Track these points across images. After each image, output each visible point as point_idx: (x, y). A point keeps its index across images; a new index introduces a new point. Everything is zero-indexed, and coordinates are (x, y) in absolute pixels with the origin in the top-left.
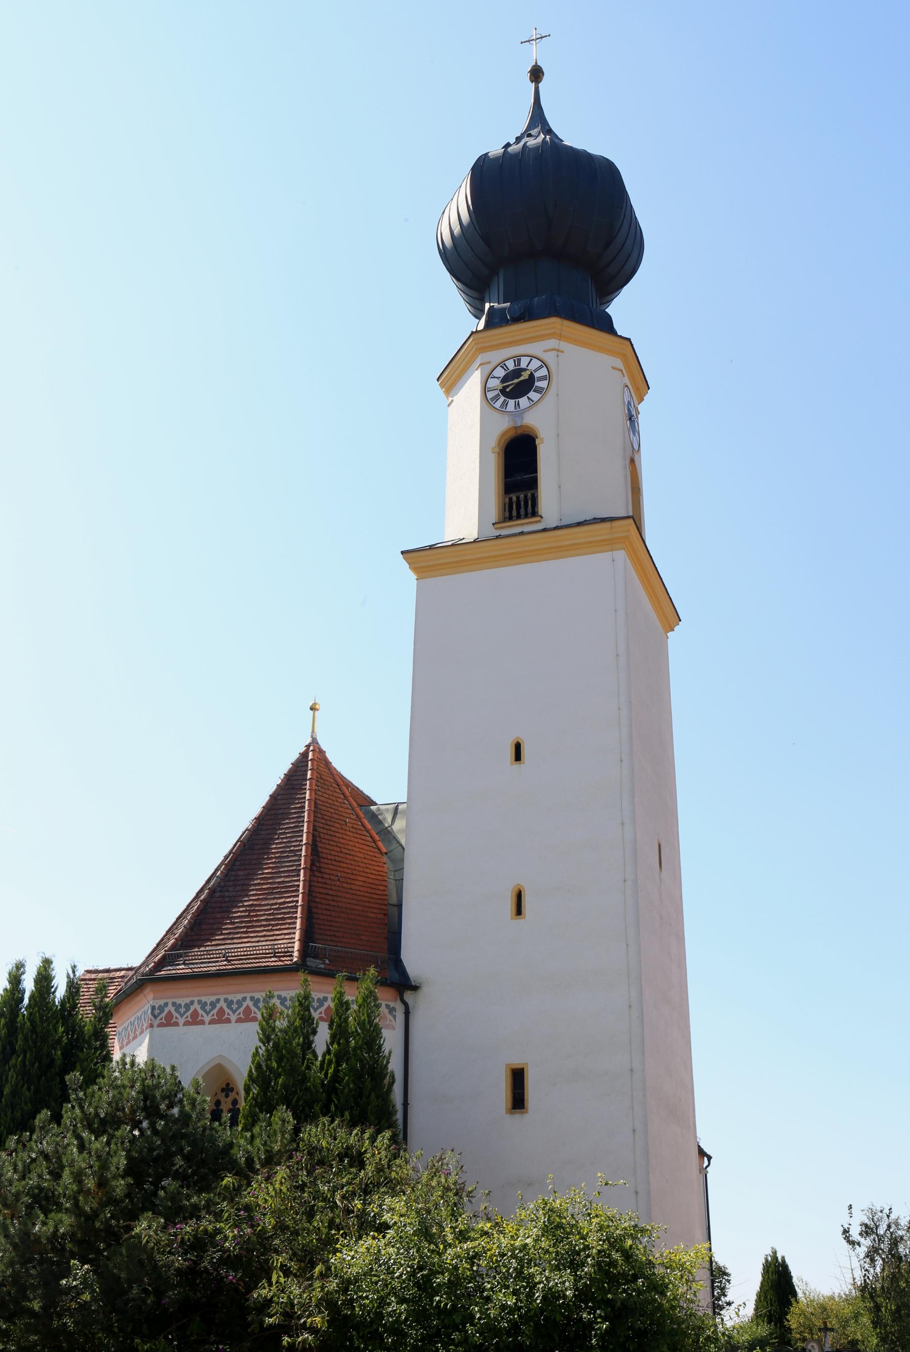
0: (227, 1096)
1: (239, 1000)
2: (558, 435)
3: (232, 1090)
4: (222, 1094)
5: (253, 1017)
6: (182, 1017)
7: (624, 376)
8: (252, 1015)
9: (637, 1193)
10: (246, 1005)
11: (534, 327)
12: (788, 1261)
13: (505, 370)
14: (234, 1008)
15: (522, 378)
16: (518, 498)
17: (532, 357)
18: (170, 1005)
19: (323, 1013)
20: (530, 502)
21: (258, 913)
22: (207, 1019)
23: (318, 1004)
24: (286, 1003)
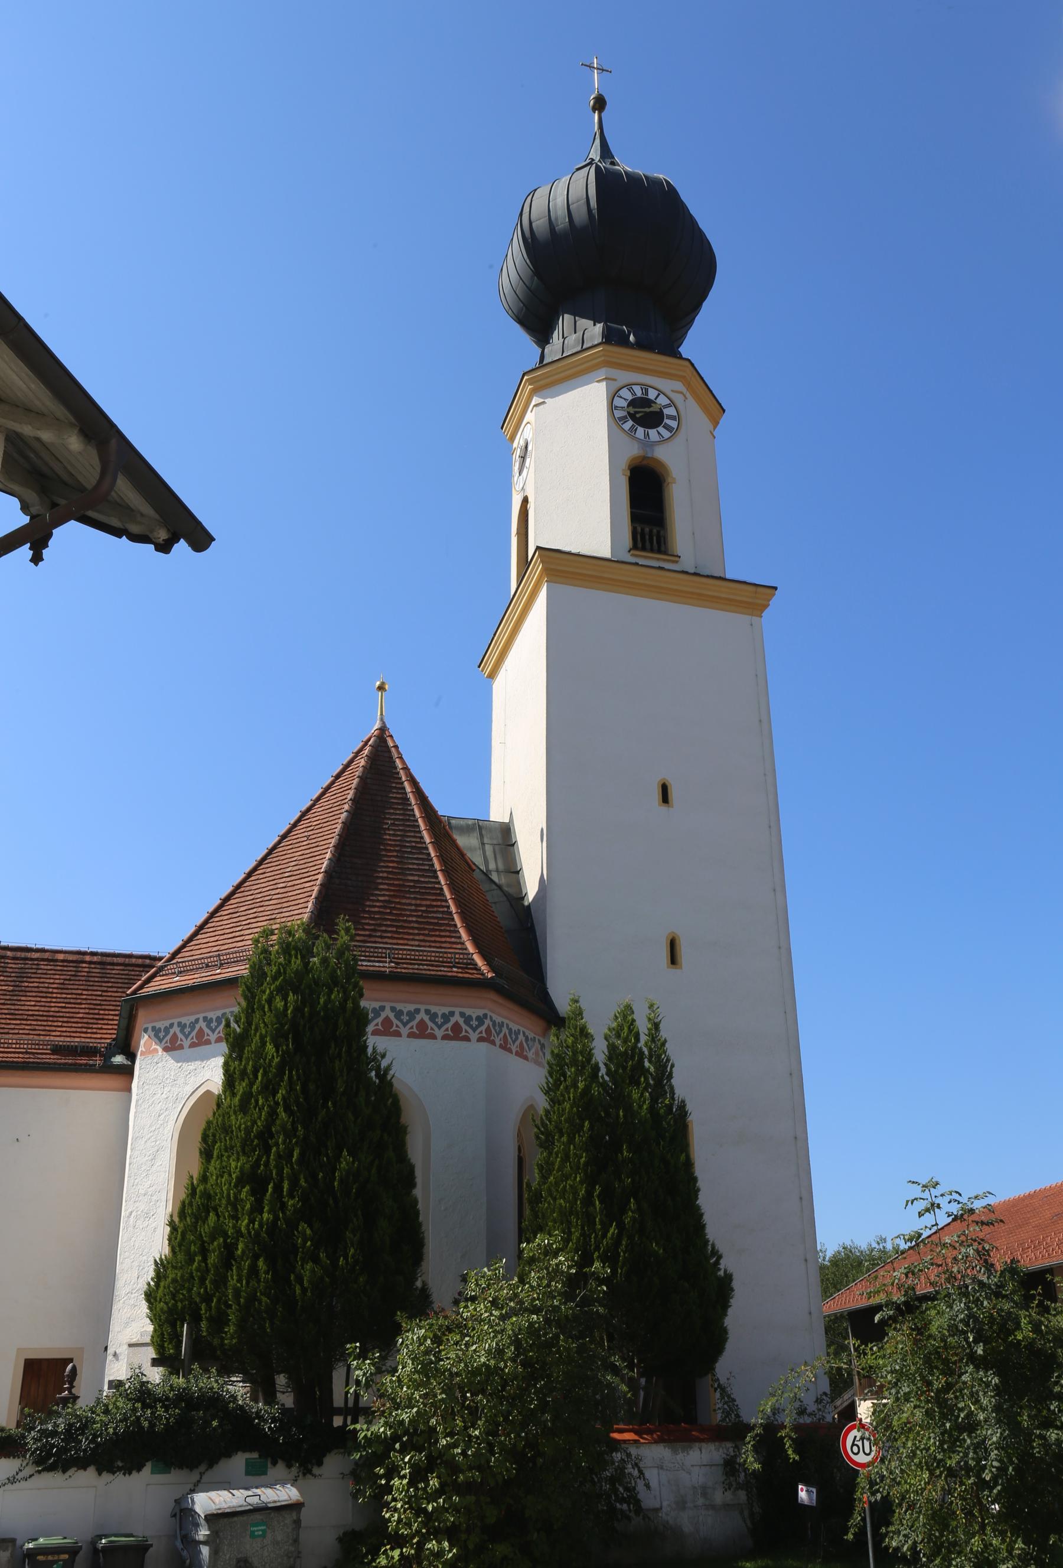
2: (690, 481)
8: (429, 1031)
9: (806, 1260)
11: (666, 362)
13: (643, 393)
15: (651, 409)
16: (651, 531)
17: (660, 392)
18: (457, 1015)
19: (380, 1024)
20: (655, 538)
21: (403, 913)
22: (439, 1033)
23: (408, 1018)
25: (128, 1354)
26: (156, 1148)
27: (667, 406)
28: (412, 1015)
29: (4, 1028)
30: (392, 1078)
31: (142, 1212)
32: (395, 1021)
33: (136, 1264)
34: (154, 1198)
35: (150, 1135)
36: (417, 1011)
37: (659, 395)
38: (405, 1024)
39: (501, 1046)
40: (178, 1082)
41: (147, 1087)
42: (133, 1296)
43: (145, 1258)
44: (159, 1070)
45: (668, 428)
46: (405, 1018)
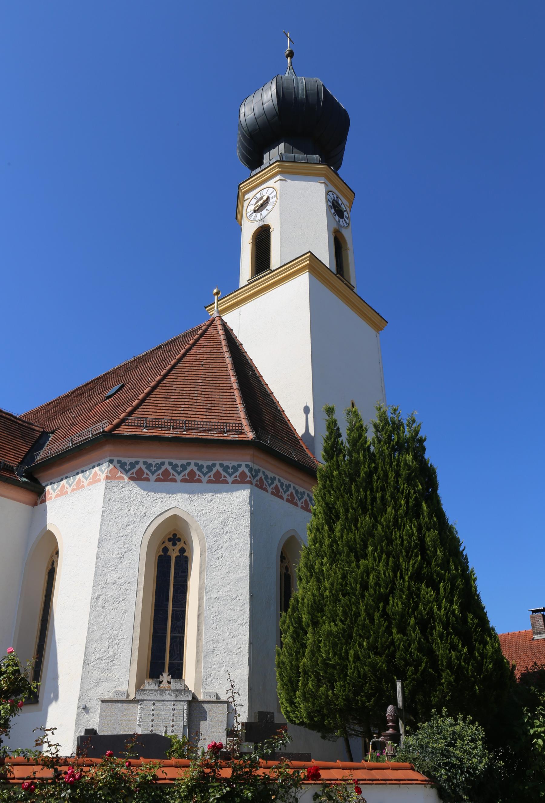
0: (174, 544)
1: (209, 465)
3: (179, 540)
4: (169, 543)
5: (188, 476)
6: (205, 476)
7: (328, 186)
10: (139, 467)
12: (468, 557)
14: (153, 470)
19: (134, 473)
23: (207, 470)
24: (203, 470)
25: (101, 710)
26: (125, 550)
28: (210, 468)
29: (2, 437)
30: (463, 550)
31: (111, 596)
32: (198, 473)
33: (106, 636)
34: (123, 587)
35: (117, 540)
36: (163, 464)
37: (274, 191)
38: (179, 474)
39: (302, 507)
40: (145, 504)
41: (112, 503)
42: (103, 661)
43: (115, 632)
44: (124, 492)
45: (272, 204)
46: (205, 470)
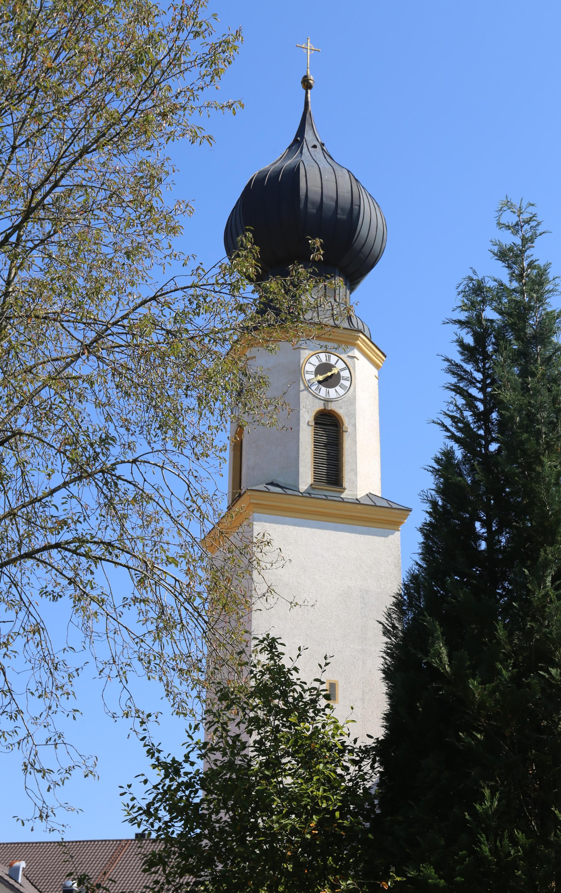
27: (346, 379)
